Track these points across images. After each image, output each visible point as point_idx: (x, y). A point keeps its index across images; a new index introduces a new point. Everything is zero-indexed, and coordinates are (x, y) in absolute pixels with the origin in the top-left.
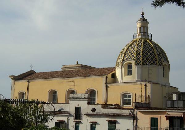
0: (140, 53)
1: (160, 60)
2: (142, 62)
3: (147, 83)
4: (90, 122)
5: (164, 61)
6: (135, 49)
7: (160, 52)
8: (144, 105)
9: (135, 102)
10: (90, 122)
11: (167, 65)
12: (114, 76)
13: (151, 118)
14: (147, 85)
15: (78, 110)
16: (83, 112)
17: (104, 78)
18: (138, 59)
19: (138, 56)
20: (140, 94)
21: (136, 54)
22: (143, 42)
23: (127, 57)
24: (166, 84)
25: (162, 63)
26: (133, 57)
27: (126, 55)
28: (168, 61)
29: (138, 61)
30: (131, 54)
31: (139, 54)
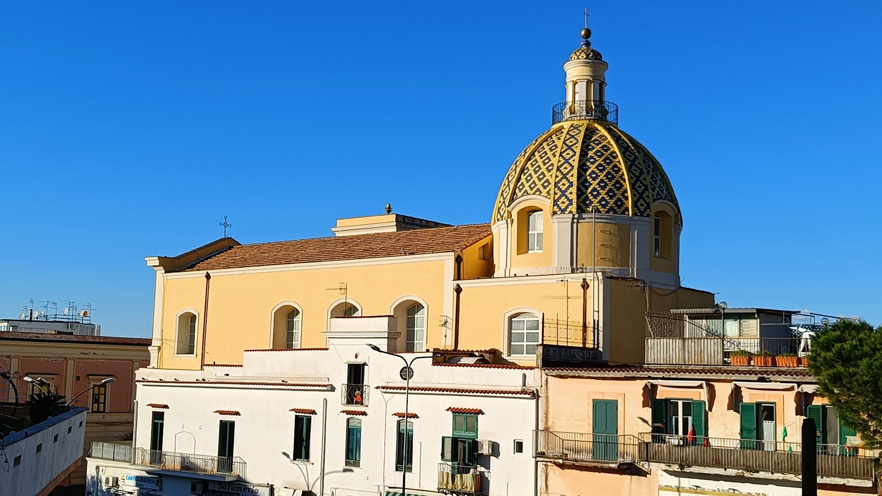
0: (569, 172)
1: (641, 197)
2: (575, 205)
3: (589, 276)
4: (395, 414)
5: (654, 200)
6: (554, 161)
7: (642, 166)
8: (579, 357)
9: (542, 345)
10: (395, 414)
11: (672, 214)
12: (488, 254)
13: (522, 452)
14: (591, 284)
15: (356, 373)
16: (370, 378)
17: (449, 259)
18: (563, 193)
19: (564, 185)
20: (563, 318)
21: (557, 176)
22: (582, 134)
23: (527, 188)
24: (214, 363)
25: (648, 207)
26: (545, 188)
27: (523, 180)
28: (673, 200)
29: (563, 203)
30: (538, 177)
31: (565, 176)
